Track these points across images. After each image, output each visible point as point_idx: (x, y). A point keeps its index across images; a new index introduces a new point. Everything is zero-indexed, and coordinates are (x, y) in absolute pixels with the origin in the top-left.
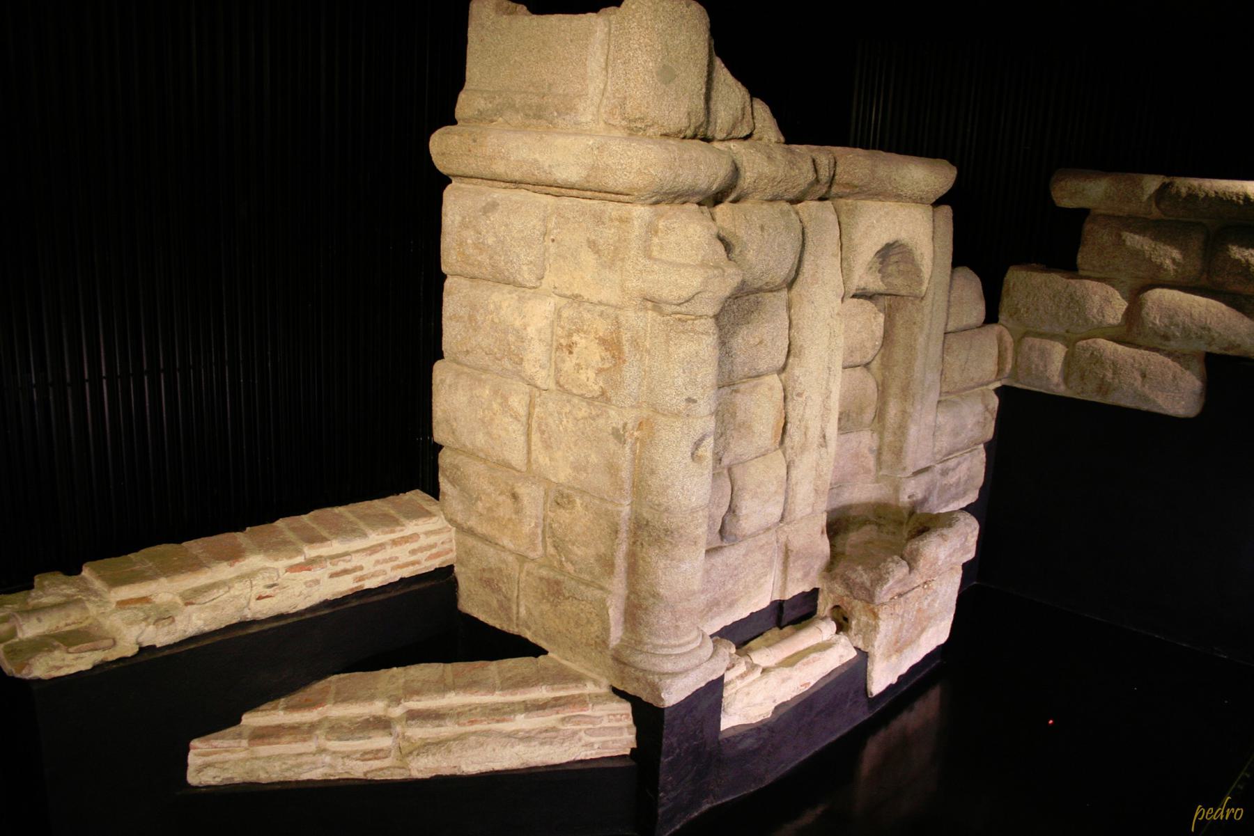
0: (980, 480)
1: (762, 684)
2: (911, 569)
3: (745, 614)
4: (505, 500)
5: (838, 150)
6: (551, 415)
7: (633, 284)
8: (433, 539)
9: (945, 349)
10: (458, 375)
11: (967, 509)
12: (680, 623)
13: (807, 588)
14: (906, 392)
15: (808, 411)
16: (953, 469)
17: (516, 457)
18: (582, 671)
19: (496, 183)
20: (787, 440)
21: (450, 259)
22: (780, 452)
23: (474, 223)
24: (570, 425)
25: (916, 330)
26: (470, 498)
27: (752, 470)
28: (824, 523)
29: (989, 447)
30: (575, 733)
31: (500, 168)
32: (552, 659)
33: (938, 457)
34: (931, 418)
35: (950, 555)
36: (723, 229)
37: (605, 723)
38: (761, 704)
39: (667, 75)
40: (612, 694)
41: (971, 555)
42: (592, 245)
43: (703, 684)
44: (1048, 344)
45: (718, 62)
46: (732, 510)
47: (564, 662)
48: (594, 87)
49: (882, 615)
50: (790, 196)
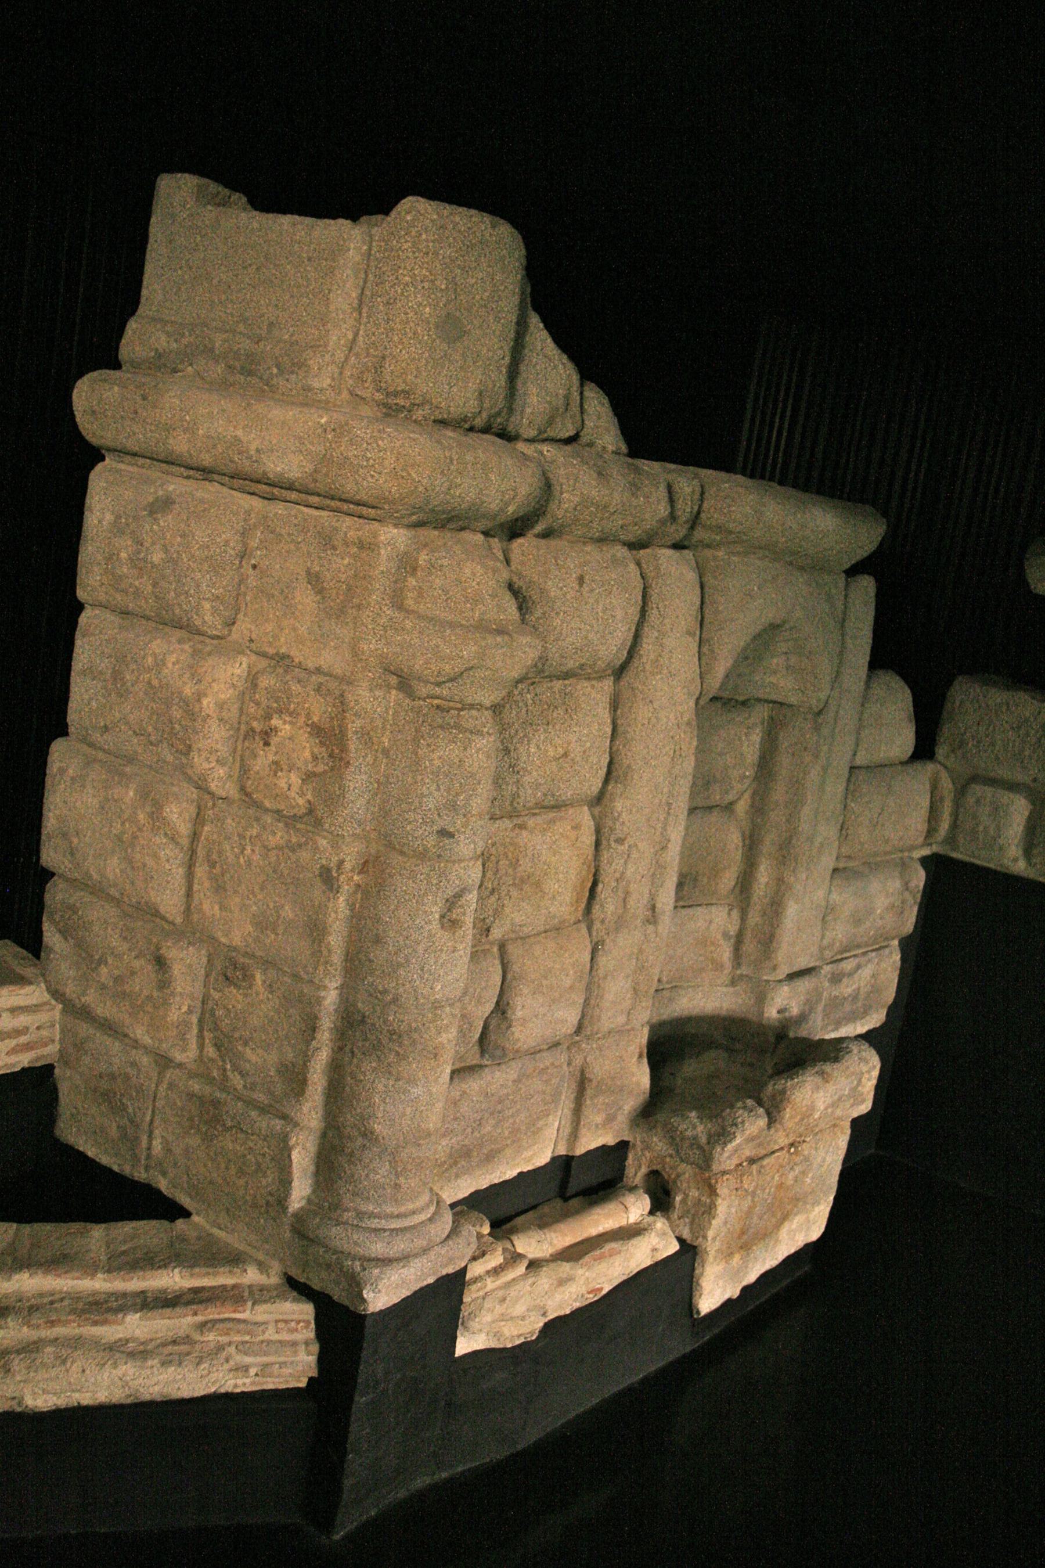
0: (890, 994)
1: (526, 1286)
2: (771, 1122)
3: (511, 1174)
4: (144, 967)
5: (708, 474)
6: (228, 838)
7: (370, 646)
8: (23, 1020)
9: (850, 792)
10: (89, 762)
11: (868, 1037)
12: (402, 1180)
13: (609, 1139)
14: (785, 854)
15: (631, 869)
16: (850, 975)
17: (169, 902)
18: (242, 1247)
19: (174, 469)
20: (596, 909)
21: (91, 581)
22: (583, 926)
23: (133, 526)
24: (256, 857)
25: (808, 759)
26: (89, 959)
27: (538, 951)
28: (644, 1041)
29: (906, 944)
30: (220, 1348)
31: (180, 444)
32: (196, 1226)
33: (828, 954)
34: (821, 893)
35: (834, 1105)
36: (520, 576)
37: (271, 1334)
38: (523, 1318)
39: (451, 328)
40: (287, 1288)
41: (865, 1107)
42: (314, 579)
43: (431, 1280)
44: (1005, 797)
45: (535, 321)
46: (501, 1008)
47: (215, 1231)
48: (337, 337)
49: (723, 1190)
50: (631, 538)
